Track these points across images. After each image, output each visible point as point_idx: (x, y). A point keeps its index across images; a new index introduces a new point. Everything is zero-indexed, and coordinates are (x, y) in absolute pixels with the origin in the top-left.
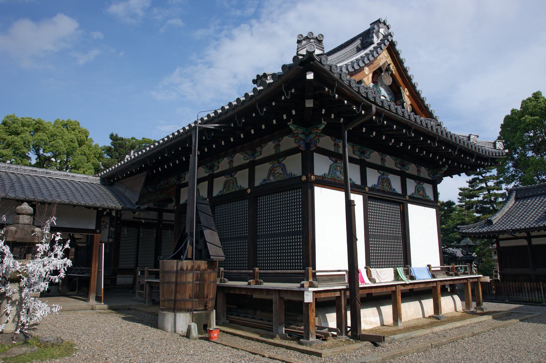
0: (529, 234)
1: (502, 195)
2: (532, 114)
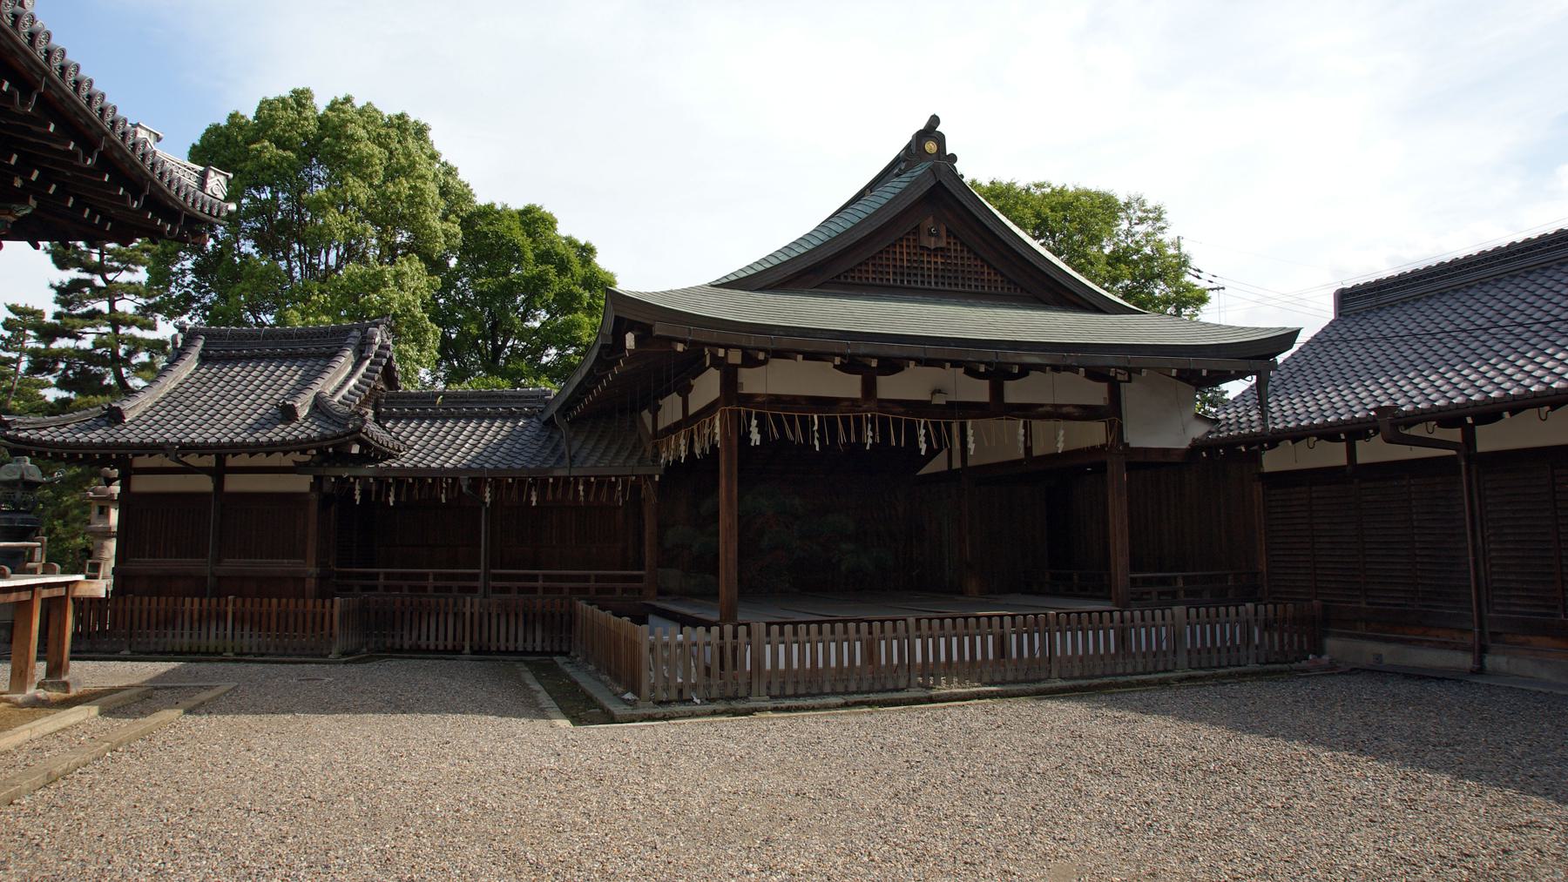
0: (221, 459)
1: (157, 347)
2: (281, 143)
